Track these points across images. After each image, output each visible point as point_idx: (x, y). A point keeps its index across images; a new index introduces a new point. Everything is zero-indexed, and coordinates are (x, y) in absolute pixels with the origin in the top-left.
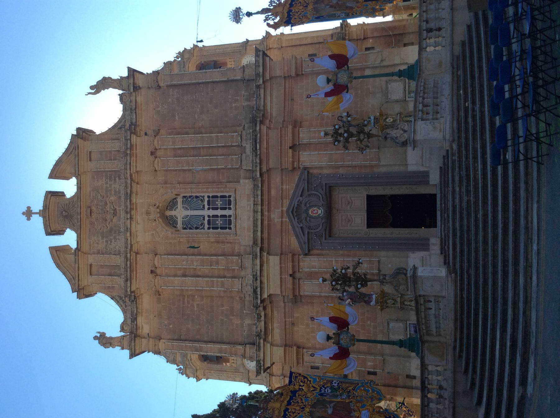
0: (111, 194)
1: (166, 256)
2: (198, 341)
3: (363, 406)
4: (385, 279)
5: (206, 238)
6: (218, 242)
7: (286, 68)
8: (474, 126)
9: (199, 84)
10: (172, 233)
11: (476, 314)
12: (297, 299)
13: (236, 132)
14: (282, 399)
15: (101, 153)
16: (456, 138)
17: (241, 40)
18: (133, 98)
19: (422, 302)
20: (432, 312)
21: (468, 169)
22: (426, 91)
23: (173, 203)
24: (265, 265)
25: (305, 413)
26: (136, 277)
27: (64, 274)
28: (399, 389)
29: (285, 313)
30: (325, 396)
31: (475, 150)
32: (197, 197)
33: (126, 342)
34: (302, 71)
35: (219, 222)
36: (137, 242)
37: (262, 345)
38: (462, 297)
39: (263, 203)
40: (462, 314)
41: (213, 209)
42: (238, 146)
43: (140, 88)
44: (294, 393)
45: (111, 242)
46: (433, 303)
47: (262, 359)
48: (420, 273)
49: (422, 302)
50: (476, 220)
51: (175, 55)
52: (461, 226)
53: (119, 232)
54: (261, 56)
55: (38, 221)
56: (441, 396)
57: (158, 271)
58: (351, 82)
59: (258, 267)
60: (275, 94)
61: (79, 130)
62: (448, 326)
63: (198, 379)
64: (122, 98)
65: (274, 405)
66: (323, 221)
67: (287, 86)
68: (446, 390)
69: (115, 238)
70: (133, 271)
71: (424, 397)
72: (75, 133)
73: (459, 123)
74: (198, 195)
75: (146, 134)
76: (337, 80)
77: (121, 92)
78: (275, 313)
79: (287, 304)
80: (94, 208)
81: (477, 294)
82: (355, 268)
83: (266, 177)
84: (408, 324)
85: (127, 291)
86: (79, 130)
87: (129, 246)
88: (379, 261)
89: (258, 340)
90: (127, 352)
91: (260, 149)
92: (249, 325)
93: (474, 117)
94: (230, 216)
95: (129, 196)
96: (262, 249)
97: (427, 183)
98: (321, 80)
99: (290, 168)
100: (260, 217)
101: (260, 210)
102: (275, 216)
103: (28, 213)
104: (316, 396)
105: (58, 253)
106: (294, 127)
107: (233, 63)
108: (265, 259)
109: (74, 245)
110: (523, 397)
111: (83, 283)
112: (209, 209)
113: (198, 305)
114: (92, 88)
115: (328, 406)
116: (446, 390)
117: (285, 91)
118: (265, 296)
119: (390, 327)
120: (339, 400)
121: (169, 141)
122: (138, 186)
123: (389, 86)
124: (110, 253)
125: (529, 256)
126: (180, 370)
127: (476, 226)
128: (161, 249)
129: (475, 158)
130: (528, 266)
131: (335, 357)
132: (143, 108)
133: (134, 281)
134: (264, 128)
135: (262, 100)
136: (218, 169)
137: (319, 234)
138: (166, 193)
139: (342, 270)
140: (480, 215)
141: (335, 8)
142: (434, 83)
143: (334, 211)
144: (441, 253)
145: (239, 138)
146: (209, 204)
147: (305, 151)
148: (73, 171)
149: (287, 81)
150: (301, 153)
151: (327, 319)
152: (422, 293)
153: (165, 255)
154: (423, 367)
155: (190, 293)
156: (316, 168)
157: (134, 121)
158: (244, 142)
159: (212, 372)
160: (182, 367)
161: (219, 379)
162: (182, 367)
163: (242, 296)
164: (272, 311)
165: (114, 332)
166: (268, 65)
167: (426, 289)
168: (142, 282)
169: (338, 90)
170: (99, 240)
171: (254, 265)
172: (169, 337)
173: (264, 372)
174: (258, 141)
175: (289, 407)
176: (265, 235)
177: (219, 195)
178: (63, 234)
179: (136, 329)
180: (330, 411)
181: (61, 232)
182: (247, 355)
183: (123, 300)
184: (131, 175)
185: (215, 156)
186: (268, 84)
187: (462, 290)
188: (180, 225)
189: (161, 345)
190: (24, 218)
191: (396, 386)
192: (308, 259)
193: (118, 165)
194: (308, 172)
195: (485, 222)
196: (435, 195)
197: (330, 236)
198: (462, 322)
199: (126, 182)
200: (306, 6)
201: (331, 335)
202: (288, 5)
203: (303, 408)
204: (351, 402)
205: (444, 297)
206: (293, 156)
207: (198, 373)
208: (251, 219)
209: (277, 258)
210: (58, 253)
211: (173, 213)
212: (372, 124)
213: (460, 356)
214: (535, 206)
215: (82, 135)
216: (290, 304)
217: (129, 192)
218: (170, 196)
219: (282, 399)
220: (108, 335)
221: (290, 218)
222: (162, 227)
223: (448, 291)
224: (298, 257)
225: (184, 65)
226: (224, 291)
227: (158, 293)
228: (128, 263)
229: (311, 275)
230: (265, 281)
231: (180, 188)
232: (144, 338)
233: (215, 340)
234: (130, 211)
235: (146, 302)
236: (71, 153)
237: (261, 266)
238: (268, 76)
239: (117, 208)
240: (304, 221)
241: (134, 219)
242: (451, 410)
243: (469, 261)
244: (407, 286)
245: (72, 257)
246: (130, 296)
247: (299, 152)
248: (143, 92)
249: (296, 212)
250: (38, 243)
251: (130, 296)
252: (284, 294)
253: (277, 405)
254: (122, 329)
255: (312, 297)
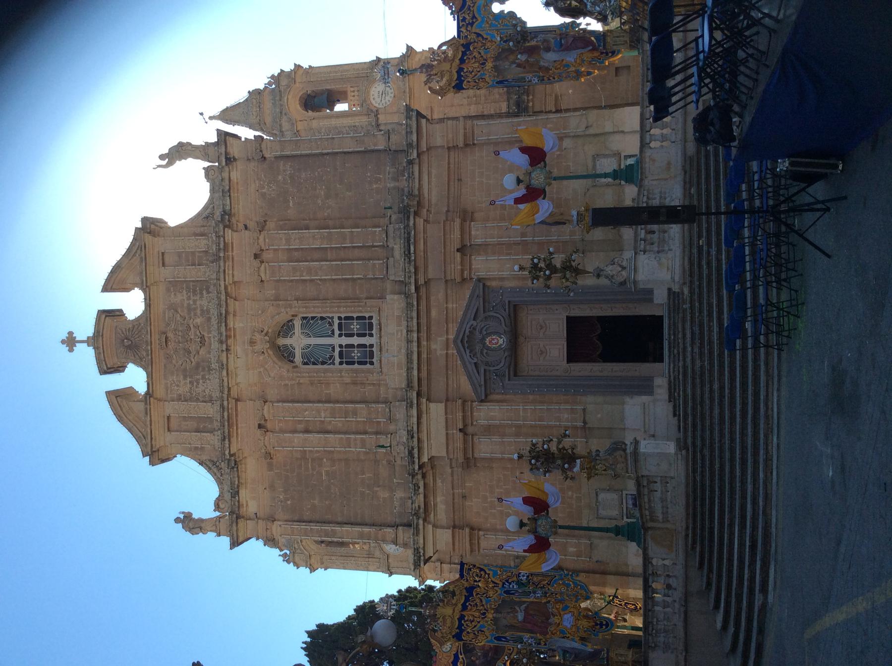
0: (195, 315)
1: (280, 404)
2: (329, 523)
3: (566, 608)
4: (598, 455)
5: (338, 378)
6: (354, 383)
7: (450, 136)
8: (710, 275)
9: (323, 154)
10: (288, 371)
11: (712, 504)
12: (469, 462)
13: (379, 227)
14: (454, 602)
15: (179, 255)
16: (688, 281)
17: (369, 57)
18: (225, 175)
19: (645, 484)
20: (658, 494)
21: (701, 325)
22: (651, 196)
23: (288, 326)
24: (424, 416)
25: (487, 622)
26: (237, 433)
27: (130, 430)
28: (609, 577)
29: (452, 483)
30: (513, 594)
31: (710, 305)
32: (322, 318)
33: (223, 525)
34: (473, 139)
35: (356, 354)
36: (237, 384)
37: (421, 527)
38: (695, 481)
39: (420, 328)
40: (695, 500)
41: (347, 335)
42: (383, 246)
43: (235, 159)
44: (470, 590)
45: (198, 383)
46: (658, 484)
47: (422, 546)
48: (642, 449)
49: (645, 484)
50: (711, 391)
51: (267, 81)
52: (694, 395)
53: (210, 369)
54: (414, 119)
55: (86, 355)
56: (669, 587)
57: (269, 425)
58: (550, 184)
59: (415, 419)
60: (434, 172)
61: (145, 220)
62: (678, 512)
63: (313, 570)
64: (207, 170)
65: (444, 610)
66: (506, 354)
67: (452, 161)
68: (675, 589)
69: (203, 377)
70: (232, 425)
71: (647, 588)
72: (139, 225)
73: (691, 264)
74: (324, 315)
75: (246, 228)
76: (530, 181)
77: (207, 164)
78: (439, 483)
79: (456, 469)
80: (171, 335)
81: (712, 480)
82: (559, 442)
83: (423, 291)
84: (624, 495)
85: (224, 454)
86: (145, 220)
87: (226, 390)
88: (584, 410)
89: (414, 521)
90: (226, 540)
91: (415, 253)
92: (401, 498)
93: (709, 264)
94: (371, 346)
95: (223, 318)
96: (419, 395)
97: (651, 300)
98: (509, 181)
99: (458, 279)
100: (415, 349)
101: (415, 339)
102: (437, 346)
103: (70, 342)
104: (500, 594)
105: (120, 400)
106: (464, 220)
107: (356, 93)
108: (424, 408)
109: (141, 387)
110: (764, 606)
111: (159, 442)
112: (340, 335)
113: (327, 472)
114: (162, 157)
115: (518, 608)
116: (675, 589)
117: (449, 168)
118: (425, 459)
119: (600, 499)
120: (532, 599)
121: (281, 239)
122: (237, 303)
123: (598, 163)
124: (197, 400)
125: (770, 448)
126: (285, 555)
127: (712, 399)
128: (272, 394)
129: (710, 315)
130: (768, 459)
131: (531, 549)
132: (241, 188)
133: (234, 440)
134: (420, 222)
135: (417, 181)
136: (354, 280)
137: (499, 371)
138: (279, 314)
139: (544, 444)
140: (716, 386)
141: (525, 68)
142: (661, 197)
143: (521, 339)
144: (670, 401)
145: (384, 236)
146: (340, 329)
147: (479, 254)
148: (138, 280)
149: (452, 153)
150: (473, 257)
151: (520, 500)
152: (645, 473)
153: (278, 402)
154: (647, 560)
155: (316, 455)
156: (494, 279)
157: (228, 208)
158: (391, 241)
159: (333, 558)
160: (288, 552)
161: (345, 568)
162: (288, 552)
163: (392, 459)
164: (434, 480)
165: (205, 510)
166: (424, 130)
167: (650, 468)
168: (246, 441)
169: (533, 194)
170: (180, 382)
171: (409, 417)
172: (286, 517)
173: (425, 564)
174: (412, 240)
175: (464, 613)
176: (424, 374)
177: (355, 315)
178: (123, 371)
179: (239, 507)
180: (521, 616)
181: (120, 369)
182: (400, 540)
183: (217, 467)
184: (226, 288)
185: (349, 260)
186: (425, 158)
187: (694, 471)
188: (298, 359)
189: (276, 529)
190: (65, 348)
191: (604, 573)
192: (485, 407)
193: (205, 272)
194: (484, 284)
195: (722, 396)
196: (662, 316)
197: (515, 375)
198: (695, 509)
199: (219, 298)
200: (484, 64)
201: (525, 521)
202: (457, 61)
203: (484, 614)
204: (549, 602)
205: (672, 478)
206: (462, 264)
207: (313, 560)
208: (404, 351)
209: (441, 407)
210: (120, 400)
211: (287, 341)
212: (575, 222)
213: (693, 548)
214: (775, 394)
215: (150, 228)
216: (460, 469)
217: (224, 312)
218: (284, 317)
219: (454, 602)
220: (196, 516)
221: (459, 352)
222: (274, 362)
223: (678, 471)
224: (471, 405)
225: (281, 96)
226: (366, 453)
227: (268, 455)
228: (226, 414)
229: (489, 430)
230: (424, 437)
231: (299, 307)
232: (250, 519)
233: (352, 520)
234: (226, 340)
235: (252, 468)
236: (134, 255)
237: (419, 418)
238: (425, 145)
239: (206, 335)
240: (478, 355)
241: (232, 351)
242: (682, 615)
243: (703, 439)
244: (627, 464)
245: (142, 406)
246: (229, 460)
247: (471, 256)
248: (240, 165)
249: (468, 342)
250: (87, 384)
251: (229, 460)
252: (451, 457)
253: (448, 611)
254: (217, 507)
255: (491, 460)
